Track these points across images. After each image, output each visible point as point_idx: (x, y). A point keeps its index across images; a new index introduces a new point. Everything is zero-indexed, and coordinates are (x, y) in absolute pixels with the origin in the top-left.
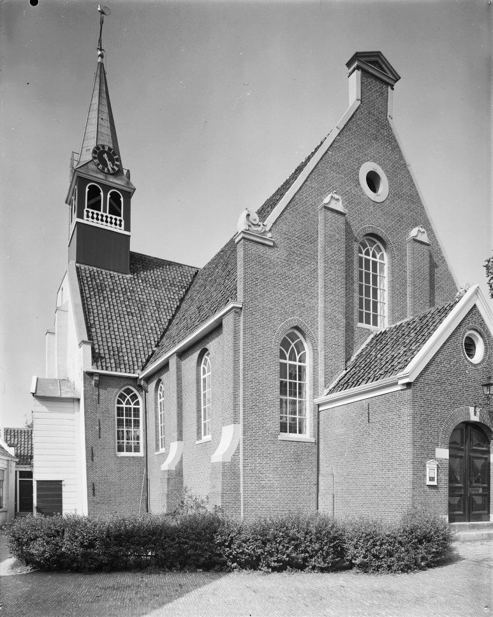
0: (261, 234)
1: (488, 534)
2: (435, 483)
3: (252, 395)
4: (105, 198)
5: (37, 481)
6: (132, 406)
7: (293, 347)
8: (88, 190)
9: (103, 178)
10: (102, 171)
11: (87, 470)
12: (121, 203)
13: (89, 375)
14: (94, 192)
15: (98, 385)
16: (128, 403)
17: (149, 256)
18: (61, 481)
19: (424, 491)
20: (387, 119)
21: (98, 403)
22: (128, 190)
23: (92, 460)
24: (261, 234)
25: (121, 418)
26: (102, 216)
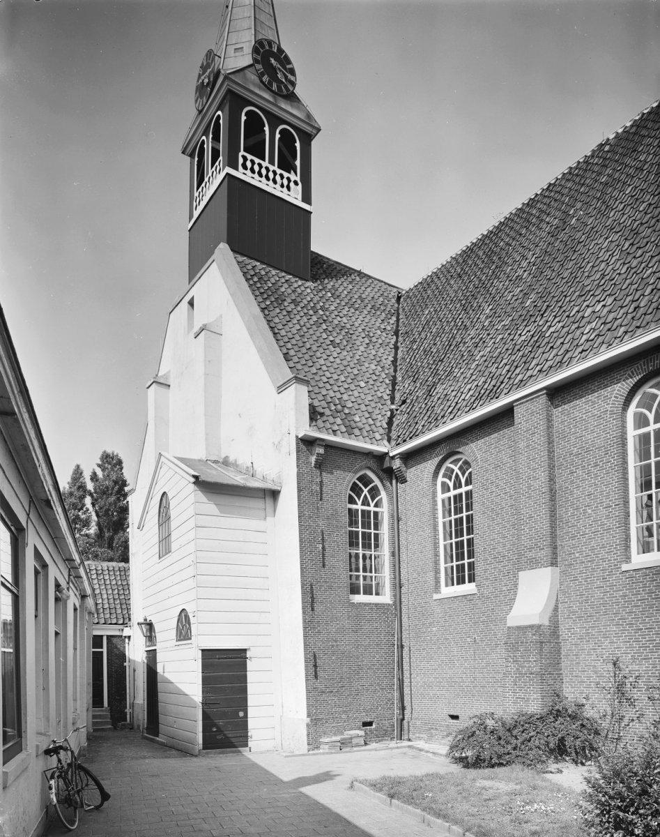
4: (271, 137)
5: (202, 650)
6: (372, 508)
7: (365, 495)
8: (245, 118)
9: (271, 99)
10: (268, 87)
11: (305, 628)
12: (296, 151)
13: (307, 443)
14: (254, 125)
15: (319, 465)
16: (365, 503)
17: (327, 259)
18: (245, 651)
21: (321, 500)
22: (308, 129)
23: (313, 610)
25: (354, 529)
26: (267, 169)
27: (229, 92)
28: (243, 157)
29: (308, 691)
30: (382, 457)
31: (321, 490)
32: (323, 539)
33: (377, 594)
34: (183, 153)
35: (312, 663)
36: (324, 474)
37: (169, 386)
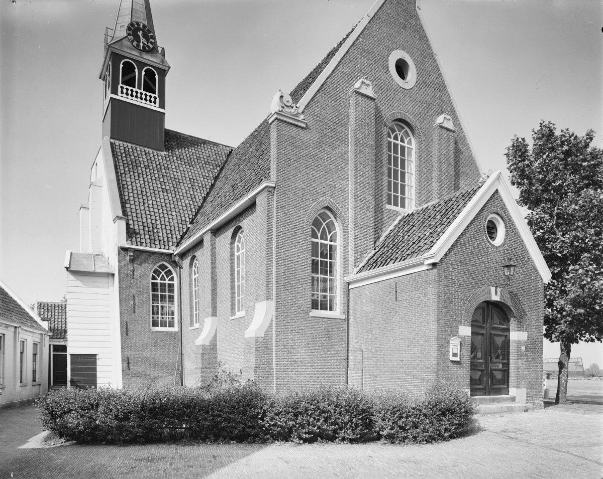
0: (294, 115)
1: (507, 407)
2: (458, 359)
3: (284, 272)
4: (139, 75)
6: (167, 282)
7: (163, 275)
9: (138, 54)
11: (122, 344)
14: (129, 68)
15: (132, 261)
18: (96, 355)
19: (448, 367)
20: (415, 10)
21: (133, 278)
23: (127, 335)
24: (294, 115)
26: (137, 92)
27: (112, 53)
28: (121, 87)
29: (123, 376)
30: (170, 255)
31: (133, 274)
32: (134, 299)
33: (331, 309)
34: (100, 78)
35: (127, 362)
36: (135, 265)
37: (89, 208)
